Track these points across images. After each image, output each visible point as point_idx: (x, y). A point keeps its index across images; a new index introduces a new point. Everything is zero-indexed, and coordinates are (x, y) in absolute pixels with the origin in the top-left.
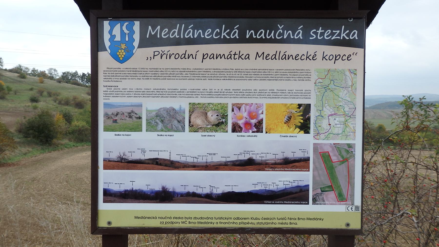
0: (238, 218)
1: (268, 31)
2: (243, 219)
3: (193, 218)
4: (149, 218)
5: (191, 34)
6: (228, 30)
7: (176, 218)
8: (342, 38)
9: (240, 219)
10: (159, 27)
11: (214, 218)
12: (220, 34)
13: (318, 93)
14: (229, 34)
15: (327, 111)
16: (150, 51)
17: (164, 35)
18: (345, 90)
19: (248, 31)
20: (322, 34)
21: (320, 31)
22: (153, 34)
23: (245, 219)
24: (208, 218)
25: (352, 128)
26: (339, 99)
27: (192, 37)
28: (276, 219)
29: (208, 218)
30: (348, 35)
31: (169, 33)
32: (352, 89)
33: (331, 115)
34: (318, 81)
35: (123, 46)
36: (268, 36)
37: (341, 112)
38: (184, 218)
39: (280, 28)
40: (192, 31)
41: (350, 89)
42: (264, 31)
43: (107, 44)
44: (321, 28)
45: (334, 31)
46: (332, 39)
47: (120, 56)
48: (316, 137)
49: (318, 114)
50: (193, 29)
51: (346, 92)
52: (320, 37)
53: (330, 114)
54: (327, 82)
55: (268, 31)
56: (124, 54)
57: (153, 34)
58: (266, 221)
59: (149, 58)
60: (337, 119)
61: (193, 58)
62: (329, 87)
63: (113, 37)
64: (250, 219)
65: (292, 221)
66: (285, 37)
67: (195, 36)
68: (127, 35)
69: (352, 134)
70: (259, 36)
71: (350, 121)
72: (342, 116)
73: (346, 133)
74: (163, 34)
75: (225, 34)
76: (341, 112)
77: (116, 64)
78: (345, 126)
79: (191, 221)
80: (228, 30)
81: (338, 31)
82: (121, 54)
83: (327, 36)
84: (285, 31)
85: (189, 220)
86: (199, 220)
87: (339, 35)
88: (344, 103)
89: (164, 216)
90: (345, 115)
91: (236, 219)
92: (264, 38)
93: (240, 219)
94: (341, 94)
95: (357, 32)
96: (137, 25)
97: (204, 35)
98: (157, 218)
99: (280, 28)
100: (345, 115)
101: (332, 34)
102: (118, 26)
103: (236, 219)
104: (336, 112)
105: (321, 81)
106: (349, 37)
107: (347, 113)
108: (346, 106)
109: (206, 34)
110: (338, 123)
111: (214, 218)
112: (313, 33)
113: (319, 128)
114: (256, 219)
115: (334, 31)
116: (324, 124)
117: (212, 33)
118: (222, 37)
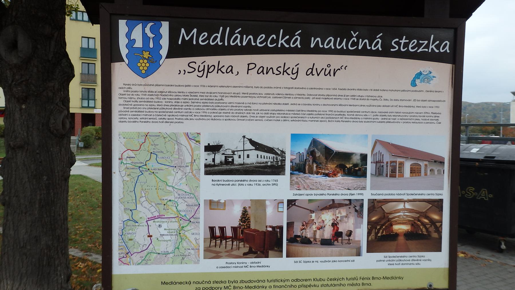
0: (297, 280)
1: (339, 39)
2: (303, 280)
3: (239, 282)
4: (180, 283)
5: (238, 41)
6: (288, 37)
7: (217, 282)
8: (430, 51)
9: (300, 280)
10: (195, 30)
11: (266, 281)
12: (277, 41)
13: (126, 178)
14: (288, 42)
15: (144, 211)
16: (182, 62)
17: (202, 41)
18: (180, 172)
19: (313, 38)
20: (406, 45)
21: (403, 41)
22: (187, 39)
23: (306, 280)
24: (259, 281)
25: (194, 242)
26: (168, 188)
27: (239, 45)
28: (345, 279)
29: (259, 281)
30: (438, 47)
31: (208, 38)
32: (191, 169)
33: (154, 218)
34: (125, 155)
35: (146, 55)
36: (339, 46)
37: (172, 212)
38: (227, 282)
39: (355, 36)
40: (239, 36)
41: (188, 169)
42: (333, 39)
43: (124, 51)
44: (404, 37)
45: (421, 42)
46: (418, 51)
47: (141, 68)
48: (123, 260)
49: (126, 217)
50: (241, 33)
51: (180, 174)
52: (404, 48)
53: (150, 216)
54: (143, 157)
55: (339, 39)
56: (139, 65)
57: (187, 39)
58: (333, 282)
59: (182, 72)
60: (165, 225)
61: (223, 73)
62: (148, 166)
63: (131, 42)
64: (313, 280)
65: (365, 282)
66: (360, 47)
67: (244, 44)
68: (151, 40)
69: (192, 252)
70: (327, 46)
71: (188, 228)
72: (173, 220)
73: (182, 250)
74: (200, 39)
75: (283, 41)
76: (172, 212)
77: (138, 79)
78: (179, 238)
79: (236, 285)
80: (288, 37)
81: (426, 42)
82: (143, 65)
83: (412, 48)
84: (361, 40)
85: (234, 284)
86: (247, 285)
87: (427, 46)
88: (176, 195)
89: (200, 281)
90: (180, 218)
91: (294, 280)
92: (333, 48)
93: (300, 280)
94: (170, 180)
95: (448, 43)
96: (165, 28)
97: (255, 41)
98: (192, 283)
99: (355, 36)
100: (180, 218)
101: (419, 45)
102: (140, 27)
103: (294, 280)
104: (163, 212)
105: (132, 154)
106: (439, 49)
107: (183, 214)
108: (180, 201)
109: (258, 41)
110: (165, 232)
111: (266, 281)
112: (395, 43)
113: (130, 243)
114: (320, 280)
115: (421, 42)
116: (140, 235)
117: (266, 40)
118: (279, 46)
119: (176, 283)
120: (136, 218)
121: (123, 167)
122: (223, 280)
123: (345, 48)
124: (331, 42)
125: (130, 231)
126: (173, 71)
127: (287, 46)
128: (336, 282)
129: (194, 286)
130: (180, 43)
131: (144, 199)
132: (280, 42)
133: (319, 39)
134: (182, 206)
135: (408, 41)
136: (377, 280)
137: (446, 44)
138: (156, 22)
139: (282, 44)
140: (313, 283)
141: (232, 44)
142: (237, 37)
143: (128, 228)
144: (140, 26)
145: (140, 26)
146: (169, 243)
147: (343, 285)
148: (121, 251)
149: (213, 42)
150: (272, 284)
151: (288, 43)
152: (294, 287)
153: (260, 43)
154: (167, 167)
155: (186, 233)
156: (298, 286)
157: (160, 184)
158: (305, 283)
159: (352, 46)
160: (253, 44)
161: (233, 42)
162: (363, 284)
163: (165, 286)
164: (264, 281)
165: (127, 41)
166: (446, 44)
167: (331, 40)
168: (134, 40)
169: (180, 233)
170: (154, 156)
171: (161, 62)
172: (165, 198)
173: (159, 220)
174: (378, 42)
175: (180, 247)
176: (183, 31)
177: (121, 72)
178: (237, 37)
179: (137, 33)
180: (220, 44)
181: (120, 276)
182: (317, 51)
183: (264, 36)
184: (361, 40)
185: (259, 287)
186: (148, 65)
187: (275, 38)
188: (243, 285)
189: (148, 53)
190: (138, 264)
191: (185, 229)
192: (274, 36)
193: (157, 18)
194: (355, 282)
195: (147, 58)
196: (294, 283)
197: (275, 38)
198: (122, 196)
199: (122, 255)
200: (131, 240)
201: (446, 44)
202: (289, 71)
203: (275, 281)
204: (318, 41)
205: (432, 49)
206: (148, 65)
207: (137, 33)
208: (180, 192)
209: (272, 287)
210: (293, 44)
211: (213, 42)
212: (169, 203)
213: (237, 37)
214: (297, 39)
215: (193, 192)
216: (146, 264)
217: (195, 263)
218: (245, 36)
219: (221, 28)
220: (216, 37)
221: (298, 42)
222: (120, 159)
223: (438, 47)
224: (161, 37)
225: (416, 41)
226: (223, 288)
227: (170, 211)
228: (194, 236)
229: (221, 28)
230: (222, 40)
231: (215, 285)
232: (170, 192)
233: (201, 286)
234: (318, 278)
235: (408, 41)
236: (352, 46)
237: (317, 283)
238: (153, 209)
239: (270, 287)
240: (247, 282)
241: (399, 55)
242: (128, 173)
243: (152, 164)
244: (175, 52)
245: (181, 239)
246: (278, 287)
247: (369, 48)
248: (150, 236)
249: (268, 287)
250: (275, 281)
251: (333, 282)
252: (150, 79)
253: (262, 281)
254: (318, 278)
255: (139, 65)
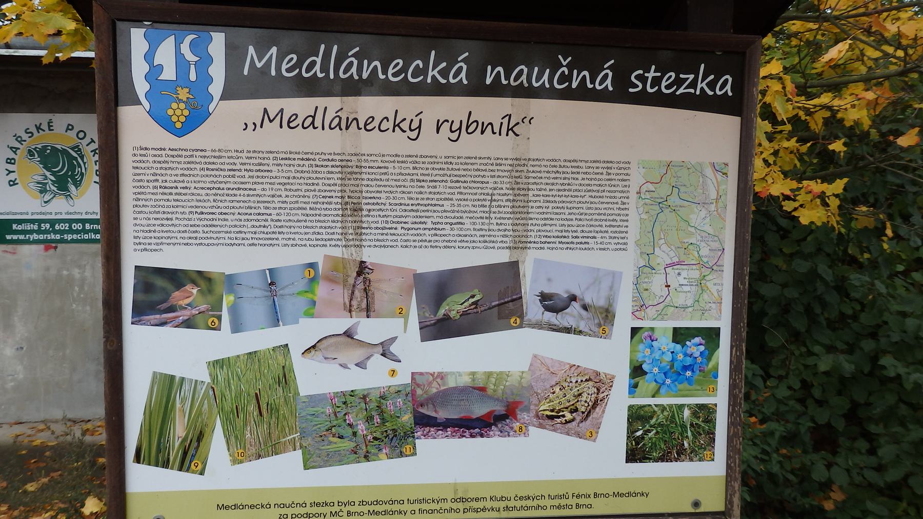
1: (536, 69)
2: (472, 500)
3: (357, 503)
4: (252, 507)
5: (354, 70)
7: (318, 505)
8: (698, 92)
9: (467, 500)
10: (274, 50)
11: (406, 502)
13: (644, 216)
14: (444, 73)
16: (252, 108)
17: (288, 70)
18: (703, 210)
19: (489, 68)
20: (656, 81)
21: (651, 75)
22: (259, 65)
23: (477, 500)
25: (716, 294)
26: (690, 229)
28: (547, 497)
31: (299, 64)
32: (716, 206)
33: (672, 265)
34: (644, 188)
35: (183, 94)
38: (336, 504)
39: (564, 63)
40: (356, 62)
41: (713, 207)
42: (526, 70)
43: (141, 87)
44: (653, 67)
45: (682, 76)
46: (678, 93)
51: (703, 213)
52: (652, 88)
53: (669, 261)
55: (536, 69)
57: (259, 65)
59: (251, 127)
60: (684, 274)
63: (154, 72)
64: (489, 499)
65: (582, 501)
66: (574, 85)
67: (365, 75)
68: (192, 67)
69: (713, 306)
71: (710, 277)
72: (694, 267)
73: (702, 304)
74: (284, 67)
75: (435, 72)
81: (692, 77)
83: (667, 87)
84: (575, 72)
85: (349, 508)
86: (372, 508)
87: (693, 85)
88: (699, 238)
89: (288, 502)
91: (456, 500)
95: (730, 80)
97: (385, 72)
98: (272, 506)
99: (564, 63)
100: (701, 265)
101: (679, 82)
102: (170, 42)
103: (456, 500)
105: (651, 187)
106: (713, 89)
107: (705, 260)
108: (703, 244)
109: (391, 71)
110: (685, 282)
111: (406, 502)
112: (636, 77)
113: (645, 294)
115: (682, 76)
117: (404, 70)
118: (429, 81)
120: (653, 264)
121: (641, 202)
122: (328, 501)
123: (547, 86)
125: (646, 280)
126: (231, 124)
127: (443, 81)
132: (430, 74)
135: (659, 74)
136: (603, 499)
137: (726, 81)
138: (200, 34)
139: (433, 77)
142: (352, 63)
143: (643, 276)
148: (635, 303)
149: (307, 71)
150: (416, 507)
151: (446, 76)
153: (394, 75)
155: (708, 284)
158: (475, 505)
164: (401, 502)
166: (727, 80)
167: (522, 70)
168: (161, 67)
169: (700, 283)
174: (606, 75)
175: (701, 299)
176: (251, 50)
178: (351, 63)
179: (166, 54)
180: (320, 75)
182: (496, 90)
183: (401, 61)
184: (575, 72)
185: (393, 513)
186: (186, 113)
187: (421, 66)
188: (365, 509)
189: (187, 90)
190: (654, 319)
195: (185, 99)
196: (455, 506)
197: (421, 66)
198: (639, 237)
199: (636, 308)
201: (726, 81)
202: (405, 126)
203: (420, 501)
204: (499, 72)
205: (702, 89)
207: (166, 54)
208: (704, 234)
209: (417, 512)
210: (454, 77)
211: (307, 72)
213: (351, 63)
215: (717, 234)
218: (366, 62)
219: (323, 47)
220: (313, 63)
221: (463, 75)
225: (673, 74)
226: (329, 514)
227: (691, 256)
228: (716, 287)
229: (323, 47)
230: (325, 69)
231: (315, 510)
233: (289, 511)
234: (499, 496)
235: (659, 74)
238: (672, 254)
239: (413, 512)
241: (642, 99)
242: (646, 210)
244: (235, 90)
246: (428, 512)
247: (590, 86)
248: (668, 286)
249: (409, 513)
250: (420, 501)
251: (524, 503)
253: (399, 502)
254: (499, 496)
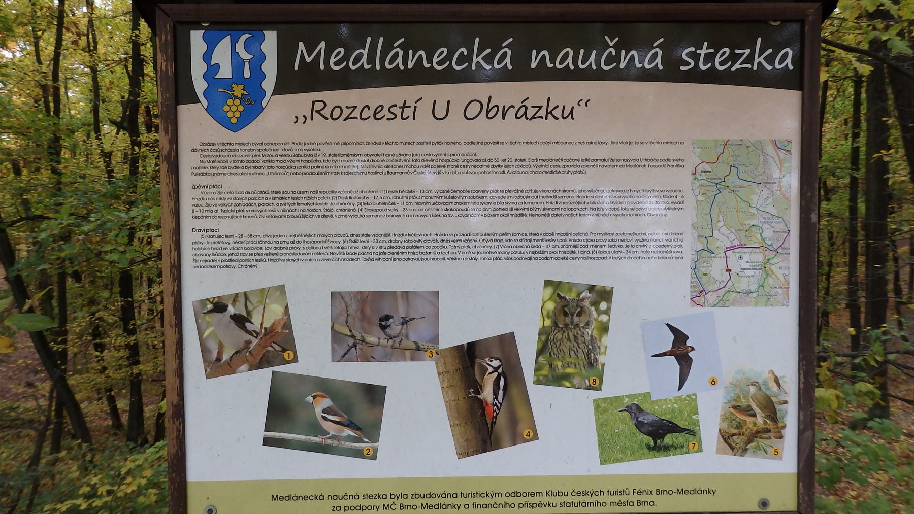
0: (516, 494)
1: (582, 51)
2: (527, 494)
3: (409, 496)
4: (305, 498)
5: (399, 60)
7: (371, 497)
8: (755, 68)
10: (323, 45)
11: (459, 495)
12: (468, 59)
13: (701, 198)
16: (302, 101)
18: (765, 190)
19: (534, 52)
20: (709, 58)
21: (703, 52)
22: (308, 60)
24: (446, 495)
25: (782, 279)
27: (402, 67)
28: (606, 493)
29: (446, 495)
31: (346, 58)
33: (733, 248)
34: (700, 169)
35: (238, 90)
38: (389, 496)
39: (611, 44)
40: (401, 53)
42: (571, 53)
43: (200, 85)
44: (706, 44)
45: (737, 51)
46: (733, 69)
48: (696, 299)
51: (765, 193)
53: (729, 245)
54: (721, 170)
55: (582, 51)
56: (226, 108)
57: (308, 60)
58: (582, 499)
59: (301, 119)
60: (746, 257)
63: (212, 70)
64: (544, 494)
65: (643, 498)
66: (622, 65)
67: (410, 65)
68: (247, 65)
69: (780, 291)
72: (757, 250)
74: (332, 60)
77: (226, 135)
78: (764, 272)
80: (489, 51)
81: (747, 52)
82: (234, 108)
83: (721, 64)
84: (623, 52)
85: (401, 501)
86: (424, 501)
87: (750, 59)
88: (762, 219)
92: (572, 67)
94: (754, 199)
96: (270, 41)
97: (430, 61)
98: (326, 497)
99: (611, 44)
100: (764, 247)
101: (734, 58)
105: (707, 167)
107: (769, 242)
108: (766, 226)
110: (747, 266)
111: (459, 495)
113: (704, 280)
114: (558, 494)
115: (737, 51)
117: (449, 58)
119: (298, 498)
121: (697, 184)
123: (594, 67)
124: (567, 58)
125: (705, 264)
126: (281, 115)
128: (587, 499)
129: (329, 504)
130: (296, 68)
131: (721, 224)
133: (545, 52)
134: (768, 233)
135: (712, 51)
136: (665, 496)
140: (545, 499)
141: (388, 67)
142: (397, 53)
143: (702, 260)
144: (228, 39)
145: (228, 39)
146: (752, 279)
147: (601, 505)
149: (354, 64)
150: (470, 501)
152: (510, 506)
153: (439, 63)
154: (750, 183)
156: (517, 506)
157: (743, 205)
158: (531, 500)
159: (606, 64)
160: (427, 66)
161: (390, 64)
162: (639, 502)
163: (278, 502)
165: (204, 67)
170: (734, 170)
171: (264, 103)
172: (746, 223)
173: (740, 250)
176: (301, 45)
177: (195, 124)
178: (397, 54)
179: (222, 54)
180: (367, 67)
181: (199, 483)
183: (445, 50)
184: (623, 52)
187: (465, 53)
190: (715, 305)
191: (772, 261)
192: (464, 50)
193: (256, 25)
194: (624, 498)
195: (239, 96)
196: (510, 500)
197: (465, 53)
198: (695, 220)
199: (695, 294)
200: (706, 275)
203: (474, 495)
205: (759, 63)
206: (241, 108)
207: (222, 54)
208: (766, 215)
209: (471, 506)
212: (753, 229)
213: (397, 54)
214: (505, 53)
215: (781, 215)
216: (724, 305)
217: (784, 305)
218: (411, 52)
219: (369, 39)
220: (359, 57)
222: (693, 174)
223: (770, 59)
224: (263, 57)
225: (727, 50)
227: (753, 238)
228: (782, 271)
229: (369, 39)
232: (753, 215)
235: (712, 51)
236: (606, 64)
237: (552, 500)
238: (732, 237)
239: (467, 506)
240: (425, 496)
242: (702, 191)
243: (732, 180)
244: (292, 81)
245: (767, 275)
246: (482, 506)
249: (462, 506)
250: (474, 495)
252: (251, 133)
253: (452, 496)
255: (226, 108)
